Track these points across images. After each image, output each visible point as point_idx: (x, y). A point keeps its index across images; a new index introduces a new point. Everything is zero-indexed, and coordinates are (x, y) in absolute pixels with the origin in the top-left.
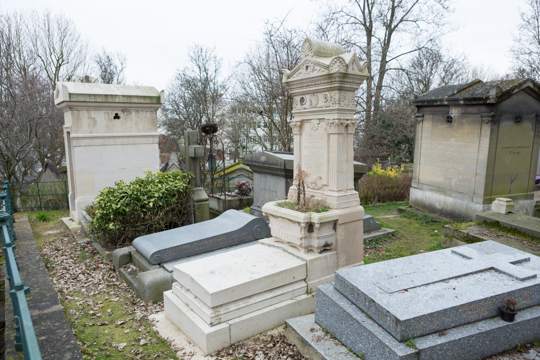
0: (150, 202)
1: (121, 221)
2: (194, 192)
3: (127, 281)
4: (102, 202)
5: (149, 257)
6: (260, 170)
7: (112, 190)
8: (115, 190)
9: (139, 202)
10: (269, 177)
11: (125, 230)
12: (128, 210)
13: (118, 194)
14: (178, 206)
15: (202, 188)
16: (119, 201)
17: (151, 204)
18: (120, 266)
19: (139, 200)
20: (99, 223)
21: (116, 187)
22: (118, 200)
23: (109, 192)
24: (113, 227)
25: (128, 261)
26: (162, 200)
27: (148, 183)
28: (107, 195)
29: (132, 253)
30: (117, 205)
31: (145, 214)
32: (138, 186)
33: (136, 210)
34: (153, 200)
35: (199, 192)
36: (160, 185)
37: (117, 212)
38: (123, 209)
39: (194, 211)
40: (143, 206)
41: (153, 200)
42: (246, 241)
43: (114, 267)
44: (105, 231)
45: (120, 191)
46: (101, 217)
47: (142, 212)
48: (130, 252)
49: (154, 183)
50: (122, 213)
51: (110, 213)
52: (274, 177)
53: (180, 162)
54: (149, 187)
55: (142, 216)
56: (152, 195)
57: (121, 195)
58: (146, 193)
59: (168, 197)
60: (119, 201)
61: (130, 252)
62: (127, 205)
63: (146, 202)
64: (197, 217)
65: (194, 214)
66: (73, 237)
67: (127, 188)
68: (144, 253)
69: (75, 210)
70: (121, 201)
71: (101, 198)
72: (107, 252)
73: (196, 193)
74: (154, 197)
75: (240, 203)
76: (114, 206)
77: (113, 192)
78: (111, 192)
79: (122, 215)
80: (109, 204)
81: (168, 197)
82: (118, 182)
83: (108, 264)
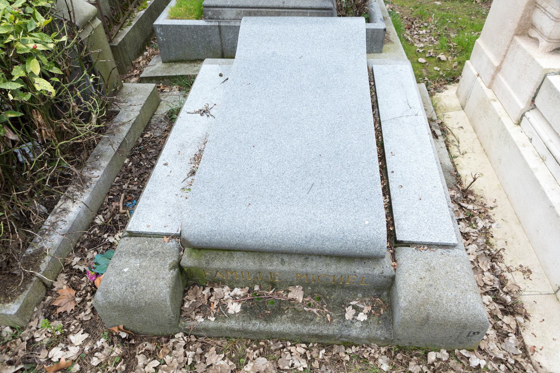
43: (125, 329)
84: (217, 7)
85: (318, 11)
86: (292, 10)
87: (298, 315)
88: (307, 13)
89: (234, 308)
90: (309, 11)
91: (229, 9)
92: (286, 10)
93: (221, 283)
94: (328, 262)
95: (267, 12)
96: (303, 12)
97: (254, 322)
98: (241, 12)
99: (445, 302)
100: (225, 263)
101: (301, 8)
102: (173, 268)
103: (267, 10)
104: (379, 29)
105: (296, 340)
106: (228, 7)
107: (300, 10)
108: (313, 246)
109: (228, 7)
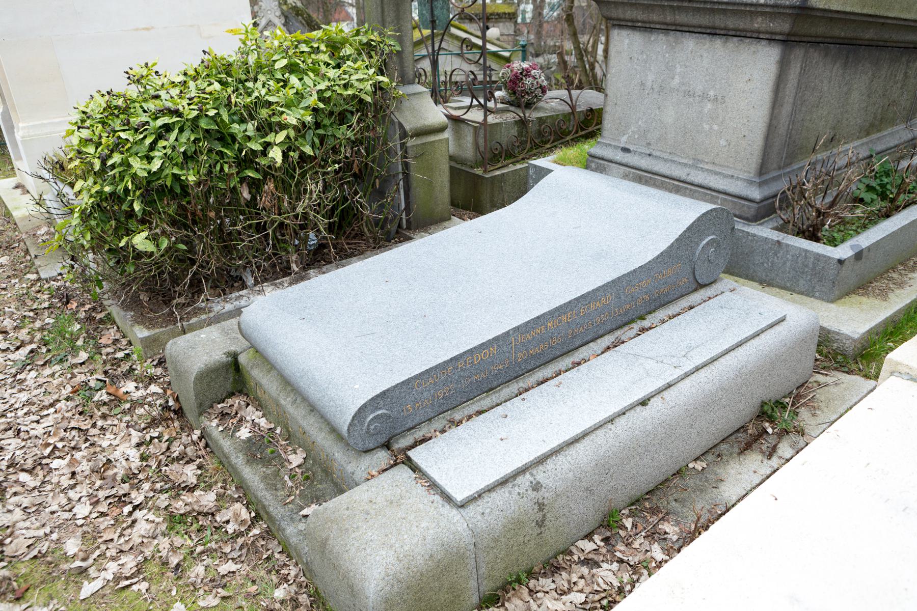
0: (267, 145)
1: (173, 223)
2: (399, 100)
3: (247, 498)
4: (91, 149)
5: (344, 421)
6: (655, 17)
7: (120, 102)
8: (129, 101)
9: (226, 145)
10: (690, 43)
11: (192, 249)
12: (192, 178)
13: (144, 118)
14: (358, 153)
15: (421, 89)
16: (152, 147)
17: (276, 154)
18: (203, 409)
19: (226, 138)
20: (91, 230)
21: (133, 91)
22: (148, 141)
23: (111, 110)
24: (150, 247)
25: (229, 387)
26: (310, 135)
27: (251, 74)
28: (104, 124)
29: (242, 359)
30: (149, 159)
31: (255, 186)
32: (217, 86)
33: (224, 177)
34: (281, 137)
35: (415, 101)
36: (294, 80)
37: (151, 189)
38: (176, 177)
39: (406, 165)
40: (247, 161)
41: (281, 137)
42: (671, 297)
43: (177, 400)
44: (123, 257)
45: (152, 106)
46: (97, 207)
47: (242, 180)
48: (235, 356)
49: (271, 73)
50: (171, 190)
51: (126, 190)
52: (718, 42)
53: (286, 17)
54: (259, 90)
55: (246, 195)
56: (275, 119)
57: (160, 122)
58: (250, 112)
59: (327, 122)
60: (152, 147)
61: (235, 356)
62: (188, 157)
63: (256, 146)
64: (414, 184)
65: (407, 177)
66: (27, 252)
67: (175, 92)
68: (331, 412)
69: (21, 159)
70: (162, 143)
71: (85, 133)
72: (142, 332)
73: (406, 104)
74: (283, 126)
75: (520, 134)
76: (138, 165)
77: (126, 110)
78: (116, 110)
79: (174, 196)
80: (116, 158)
81: (327, 122)
82: (138, 71)
83: (152, 379)
84: (602, 159)
85: (735, 200)
86: (697, 188)
87: (273, 481)
88: (718, 198)
89: (244, 433)
90: (721, 196)
91: (617, 166)
92: (689, 186)
93: (260, 406)
94: (323, 427)
95: (662, 182)
96: (712, 196)
97: (240, 455)
98: (630, 173)
99: (353, 536)
100: (261, 375)
101: (710, 189)
102: (228, 354)
103: (663, 179)
104: (830, 258)
105: (247, 498)
106: (616, 163)
107: (709, 192)
108: (302, 384)
109: (616, 163)
